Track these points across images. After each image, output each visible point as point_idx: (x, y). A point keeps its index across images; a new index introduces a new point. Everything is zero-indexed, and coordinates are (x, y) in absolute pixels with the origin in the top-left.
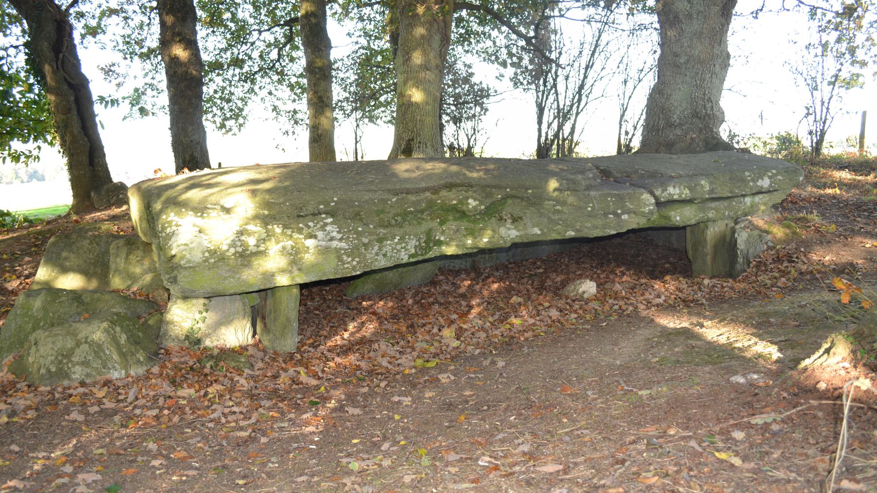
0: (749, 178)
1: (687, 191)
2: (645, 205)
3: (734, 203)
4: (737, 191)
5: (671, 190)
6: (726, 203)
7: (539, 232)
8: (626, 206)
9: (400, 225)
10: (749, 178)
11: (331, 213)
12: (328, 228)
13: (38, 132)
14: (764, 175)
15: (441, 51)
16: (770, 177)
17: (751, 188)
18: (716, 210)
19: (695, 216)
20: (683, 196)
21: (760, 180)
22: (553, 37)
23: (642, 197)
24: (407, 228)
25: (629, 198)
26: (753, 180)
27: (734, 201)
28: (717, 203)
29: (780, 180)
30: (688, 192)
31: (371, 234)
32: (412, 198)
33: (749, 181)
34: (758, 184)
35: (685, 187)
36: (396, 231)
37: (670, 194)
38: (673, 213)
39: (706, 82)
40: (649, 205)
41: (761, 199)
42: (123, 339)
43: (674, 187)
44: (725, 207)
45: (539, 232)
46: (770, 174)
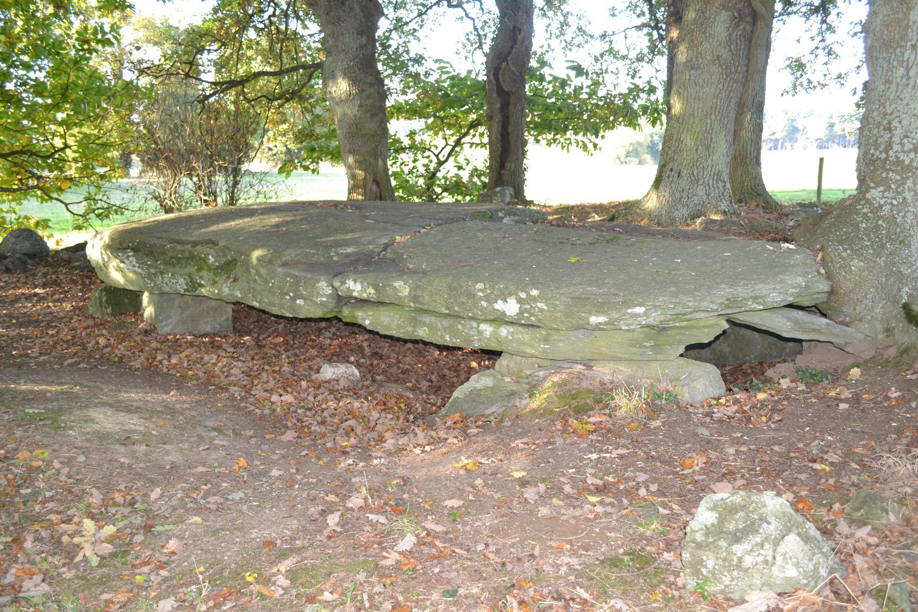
0: (480, 294)
1: (371, 291)
2: (318, 294)
3: (460, 327)
4: (457, 309)
5: (350, 284)
6: (445, 323)
7: (239, 296)
8: (299, 290)
9: (173, 264)
10: (480, 294)
11: (135, 250)
12: (131, 259)
13: (335, 156)
14: (510, 294)
15: (730, 35)
16: (520, 301)
17: (482, 309)
18: (431, 327)
19: (399, 326)
20: (365, 295)
21: (500, 302)
22: (473, 76)
23: (317, 285)
24: (177, 269)
25: (305, 283)
26: (487, 298)
27: (460, 323)
28: (433, 319)
29: (541, 310)
30: (373, 291)
31: (156, 268)
32: (179, 247)
33: (481, 299)
34: (497, 306)
35: (369, 284)
36: (171, 269)
37: (348, 289)
38: (360, 314)
39: (893, 87)
40: (322, 296)
41: (512, 334)
42: (104, 299)
43: (355, 281)
44: (445, 329)
45: (239, 296)
46: (523, 295)
